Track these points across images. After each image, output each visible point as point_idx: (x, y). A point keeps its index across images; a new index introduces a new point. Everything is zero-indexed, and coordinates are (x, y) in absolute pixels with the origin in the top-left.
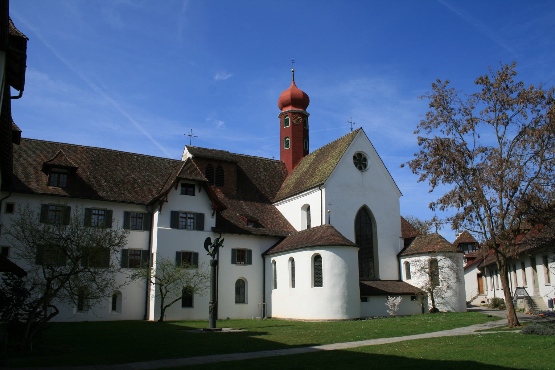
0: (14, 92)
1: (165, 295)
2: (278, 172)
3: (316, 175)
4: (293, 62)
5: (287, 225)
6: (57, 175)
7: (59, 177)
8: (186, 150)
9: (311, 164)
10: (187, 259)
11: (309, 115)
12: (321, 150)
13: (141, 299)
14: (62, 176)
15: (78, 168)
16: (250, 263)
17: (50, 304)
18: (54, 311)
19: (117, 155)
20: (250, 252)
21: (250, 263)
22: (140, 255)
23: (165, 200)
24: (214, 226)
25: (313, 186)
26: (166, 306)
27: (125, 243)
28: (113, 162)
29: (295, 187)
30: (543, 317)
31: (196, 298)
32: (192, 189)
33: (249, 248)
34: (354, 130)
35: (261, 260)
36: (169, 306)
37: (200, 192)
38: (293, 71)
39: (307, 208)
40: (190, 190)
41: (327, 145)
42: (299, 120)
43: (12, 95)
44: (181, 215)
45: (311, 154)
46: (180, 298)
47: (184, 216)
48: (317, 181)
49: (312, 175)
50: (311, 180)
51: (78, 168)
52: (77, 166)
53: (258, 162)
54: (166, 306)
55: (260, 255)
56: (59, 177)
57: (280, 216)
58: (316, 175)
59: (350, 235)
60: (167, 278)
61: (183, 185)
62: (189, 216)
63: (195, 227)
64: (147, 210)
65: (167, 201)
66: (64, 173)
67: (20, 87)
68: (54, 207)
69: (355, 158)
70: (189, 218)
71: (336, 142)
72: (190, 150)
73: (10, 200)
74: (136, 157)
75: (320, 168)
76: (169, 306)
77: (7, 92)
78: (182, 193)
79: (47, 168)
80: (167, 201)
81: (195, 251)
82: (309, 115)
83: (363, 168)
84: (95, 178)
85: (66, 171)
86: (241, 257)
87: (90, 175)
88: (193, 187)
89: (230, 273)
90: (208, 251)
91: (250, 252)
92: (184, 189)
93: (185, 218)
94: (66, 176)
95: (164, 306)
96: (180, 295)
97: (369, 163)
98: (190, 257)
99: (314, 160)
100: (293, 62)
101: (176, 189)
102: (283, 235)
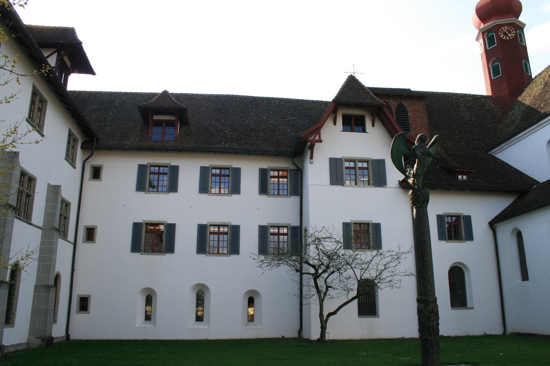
1: (325, 293)
10: (364, 235)
11: (524, 25)
17: (65, 339)
20: (468, 219)
21: (470, 237)
22: (146, 232)
23: (317, 138)
26: (330, 314)
27: (79, 155)
31: (384, 297)
33: (465, 213)
35: (490, 233)
36: (334, 313)
37: (373, 126)
42: (507, 35)
44: (347, 164)
46: (353, 299)
47: (352, 164)
53: (457, 99)
54: (330, 314)
55: (486, 224)
60: (326, 261)
62: (360, 165)
63: (371, 182)
64: (293, 163)
65: (320, 141)
68: (157, 168)
70: (360, 168)
73: (96, 161)
76: (334, 313)
80: (320, 141)
81: (375, 221)
82: (524, 25)
91: (468, 219)
93: (354, 168)
95: (325, 314)
96: (354, 293)
98: (368, 230)
101: (335, 124)
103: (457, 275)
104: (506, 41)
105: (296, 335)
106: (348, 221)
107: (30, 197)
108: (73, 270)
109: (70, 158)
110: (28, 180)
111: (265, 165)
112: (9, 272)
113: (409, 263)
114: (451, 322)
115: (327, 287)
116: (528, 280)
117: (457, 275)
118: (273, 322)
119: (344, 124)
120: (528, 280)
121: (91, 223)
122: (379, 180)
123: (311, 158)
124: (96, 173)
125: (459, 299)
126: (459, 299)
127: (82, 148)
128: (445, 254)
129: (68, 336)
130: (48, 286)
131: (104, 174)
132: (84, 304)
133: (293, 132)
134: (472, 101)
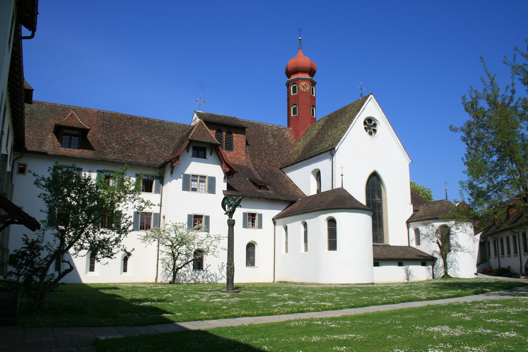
0: (25, 32)
2: (285, 138)
3: (325, 140)
4: (300, 30)
5: (296, 190)
6: (68, 137)
7: (70, 140)
8: (195, 116)
9: (319, 130)
10: (197, 221)
12: (329, 116)
13: (129, 265)
14: (73, 138)
15: (89, 130)
16: (260, 226)
18: (67, 267)
19: (128, 119)
24: (226, 189)
25: (323, 151)
28: (124, 125)
29: (304, 152)
30: (443, 285)
31: (207, 260)
32: (203, 152)
34: (363, 96)
38: (300, 40)
39: (318, 174)
40: (201, 153)
41: (336, 112)
43: (23, 35)
45: (319, 121)
48: (327, 146)
49: (321, 141)
50: (321, 145)
51: (89, 130)
52: (88, 128)
53: (267, 128)
56: (70, 140)
57: (289, 181)
58: (325, 140)
59: (361, 198)
61: (194, 148)
63: (207, 190)
66: (75, 135)
67: (32, 27)
69: (365, 123)
71: (345, 108)
72: (200, 115)
73: (23, 161)
74: (146, 121)
75: (330, 134)
77: (18, 31)
78: (193, 156)
79: (60, 131)
83: (373, 133)
84: (106, 140)
85: (77, 133)
86: (251, 219)
87: (102, 137)
88: (204, 150)
89: (243, 235)
90: (225, 210)
92: (196, 152)
94: (77, 138)
97: (379, 128)
99: (322, 126)
100: (300, 30)
101: (188, 152)
102: (294, 199)
103: (251, 247)
104: (303, 92)
105: (408, 245)
106: (191, 214)
111: (200, 277)
112: (481, 297)
113: (225, 243)
114: (243, 275)
115: (179, 254)
117: (251, 247)
118: (47, 274)
119: (193, 149)
122: (212, 189)
123: (172, 173)
125: (250, 260)
126: (250, 260)
128: (243, 235)
133: (158, 148)
134: (277, 130)
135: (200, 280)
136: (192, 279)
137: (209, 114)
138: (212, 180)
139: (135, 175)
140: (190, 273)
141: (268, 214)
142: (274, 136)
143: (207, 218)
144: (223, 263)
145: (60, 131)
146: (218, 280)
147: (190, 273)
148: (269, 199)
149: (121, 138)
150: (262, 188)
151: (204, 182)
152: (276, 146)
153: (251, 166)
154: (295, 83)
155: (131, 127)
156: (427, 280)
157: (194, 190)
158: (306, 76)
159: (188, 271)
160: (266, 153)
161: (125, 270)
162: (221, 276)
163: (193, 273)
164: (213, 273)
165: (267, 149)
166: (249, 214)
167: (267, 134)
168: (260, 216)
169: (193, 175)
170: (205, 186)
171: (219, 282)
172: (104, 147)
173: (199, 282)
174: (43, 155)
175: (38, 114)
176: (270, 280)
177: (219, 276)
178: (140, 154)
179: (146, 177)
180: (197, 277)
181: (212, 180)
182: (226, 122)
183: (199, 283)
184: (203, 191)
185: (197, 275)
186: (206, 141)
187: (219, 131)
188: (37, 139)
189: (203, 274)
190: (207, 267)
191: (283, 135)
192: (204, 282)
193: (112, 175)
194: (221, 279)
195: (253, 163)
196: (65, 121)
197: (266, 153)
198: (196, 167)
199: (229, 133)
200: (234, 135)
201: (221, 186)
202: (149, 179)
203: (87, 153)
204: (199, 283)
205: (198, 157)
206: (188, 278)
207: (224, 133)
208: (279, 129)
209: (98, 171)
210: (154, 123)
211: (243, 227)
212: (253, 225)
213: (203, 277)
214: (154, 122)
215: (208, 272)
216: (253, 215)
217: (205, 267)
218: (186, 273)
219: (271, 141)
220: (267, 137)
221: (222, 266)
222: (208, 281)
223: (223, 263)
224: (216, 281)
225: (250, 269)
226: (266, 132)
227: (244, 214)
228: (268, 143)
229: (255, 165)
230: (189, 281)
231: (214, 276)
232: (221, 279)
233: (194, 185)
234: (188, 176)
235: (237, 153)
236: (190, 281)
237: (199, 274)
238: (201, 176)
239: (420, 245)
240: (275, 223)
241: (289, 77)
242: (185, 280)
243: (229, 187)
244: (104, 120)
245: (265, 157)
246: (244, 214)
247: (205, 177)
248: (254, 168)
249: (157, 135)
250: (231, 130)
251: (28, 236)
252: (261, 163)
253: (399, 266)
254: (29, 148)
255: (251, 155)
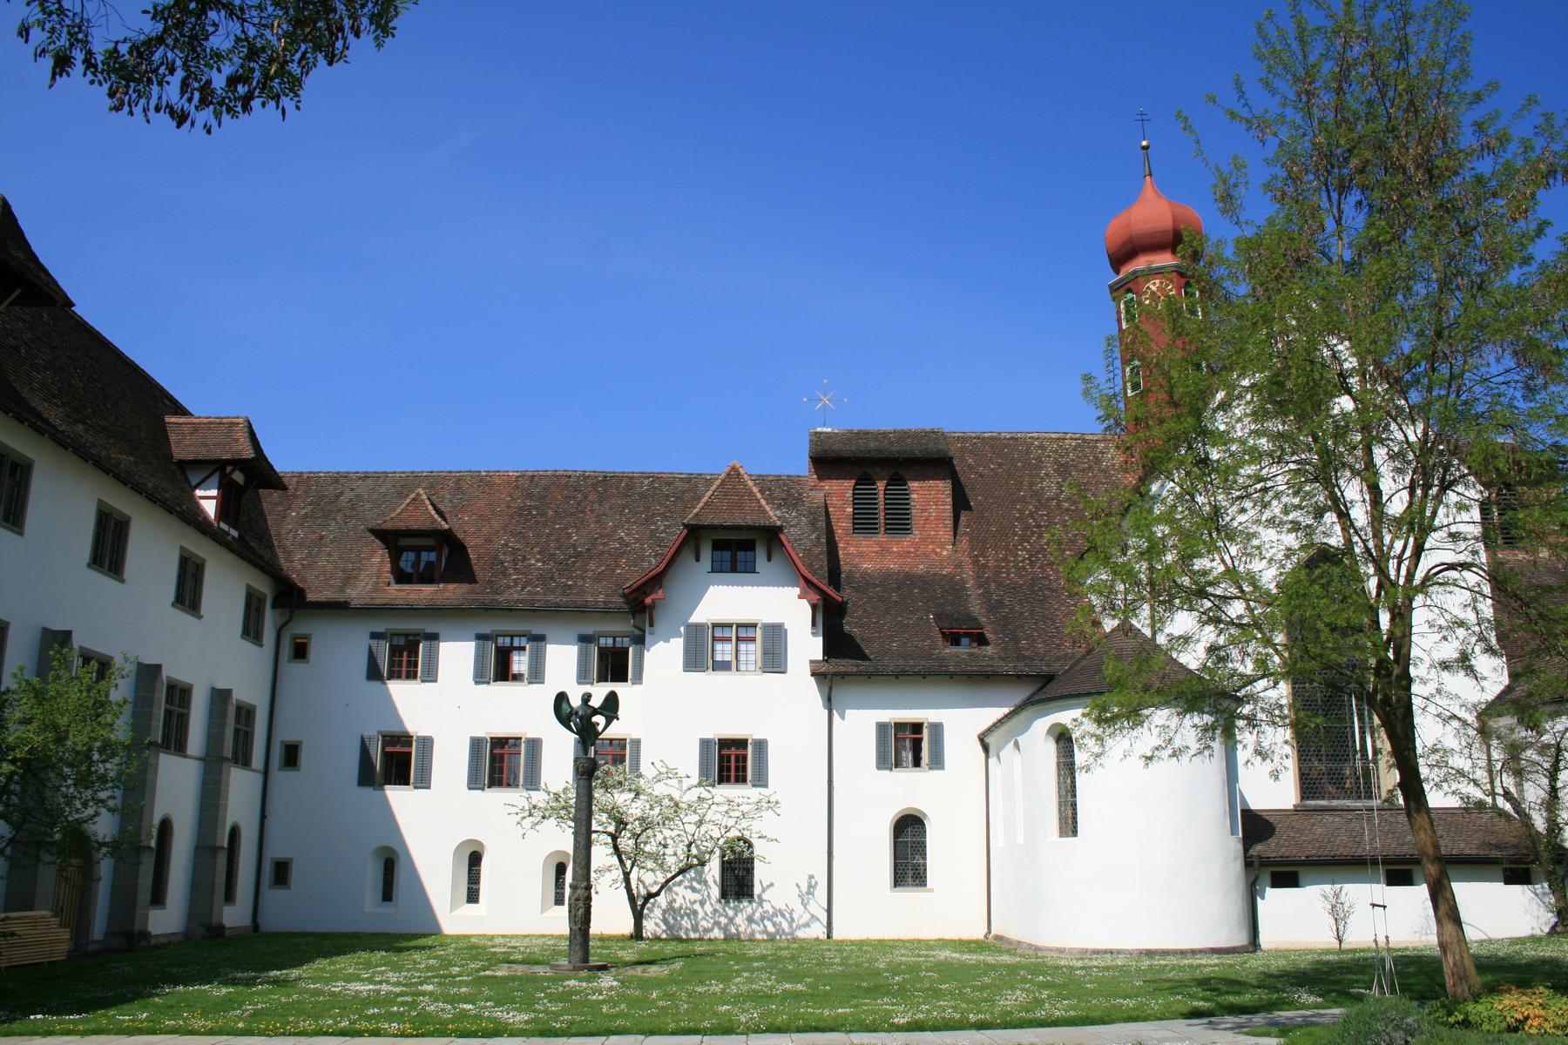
16: (937, 762)
19: (595, 486)
24: (819, 656)
27: (270, 620)
37: (769, 560)
61: (718, 546)
73: (302, 627)
84: (515, 551)
100: (1142, 118)
101: (698, 560)
103: (909, 829)
107: (183, 721)
108: (263, 817)
109: (252, 631)
110: (180, 694)
111: (741, 918)
116: (942, 767)
117: (909, 829)
119: (714, 549)
120: (942, 767)
121: (291, 737)
122: (774, 660)
124: (300, 652)
127: (274, 606)
129: (256, 926)
130: (217, 851)
131: (313, 651)
132: (282, 873)
134: (1075, 449)
135: (741, 929)
136: (717, 923)
137: (851, 432)
138: (775, 637)
139: (575, 638)
140: (708, 908)
141: (961, 722)
142: (1063, 470)
143: (761, 745)
144: (811, 877)
145: (392, 539)
146: (799, 927)
147: (708, 908)
148: (956, 674)
149: (558, 540)
150: (965, 641)
151: (753, 640)
152: (1068, 499)
153: (968, 573)
154: (1129, 291)
155: (596, 506)
156: (250, 983)
157: (723, 666)
158: (1165, 260)
159: (702, 903)
160: (1027, 527)
161: (473, 897)
162: (807, 917)
163: (718, 906)
164: (780, 905)
165: (1031, 515)
166: (900, 726)
167: (1038, 467)
168: (937, 729)
169: (715, 625)
170: (752, 652)
171: (800, 934)
172: (505, 575)
173: (739, 933)
174: (338, 609)
175: (368, 506)
176: (977, 932)
177: (801, 915)
178: (598, 579)
179: (610, 641)
180: (731, 920)
181: (775, 637)
182: (847, 450)
183: (737, 937)
184: (752, 667)
185: (731, 913)
186: (740, 522)
187: (865, 480)
188: (343, 571)
189: (749, 910)
190: (764, 890)
191: (1097, 460)
192: (753, 934)
193: (516, 644)
194: (807, 925)
195: (976, 562)
196: (398, 516)
197: (1027, 527)
198: (724, 600)
199: (897, 480)
200: (914, 485)
201: (806, 646)
202: (618, 645)
203: (450, 592)
204: (739, 940)
205: (734, 570)
206: (704, 923)
207: (881, 485)
208: (1084, 443)
209: (480, 637)
210: (668, 484)
211: (879, 768)
212: (917, 763)
213: (750, 920)
214: (669, 481)
215: (766, 906)
216: (917, 727)
217: (757, 890)
218: (697, 906)
219: (1050, 486)
220: (1037, 475)
221: (810, 886)
222: (765, 931)
223: (811, 877)
224: (792, 934)
225: (909, 895)
226: (1039, 459)
227: (882, 728)
228: (1038, 495)
229: (980, 568)
230: (706, 930)
231: (783, 916)
232: (807, 925)
233: (724, 651)
234: (699, 628)
235: (923, 540)
236: (711, 930)
237: (737, 911)
238: (739, 626)
239: (1075, 833)
240: (986, 748)
241: (1118, 273)
242: (695, 928)
243: (830, 650)
244: (530, 496)
245: (1023, 539)
246: (882, 728)
247: (754, 626)
248: (978, 577)
249: (665, 518)
250: (902, 472)
251: (1097, 771)
252: (1005, 559)
253: (1508, 881)
254: (311, 597)
255: (971, 541)
